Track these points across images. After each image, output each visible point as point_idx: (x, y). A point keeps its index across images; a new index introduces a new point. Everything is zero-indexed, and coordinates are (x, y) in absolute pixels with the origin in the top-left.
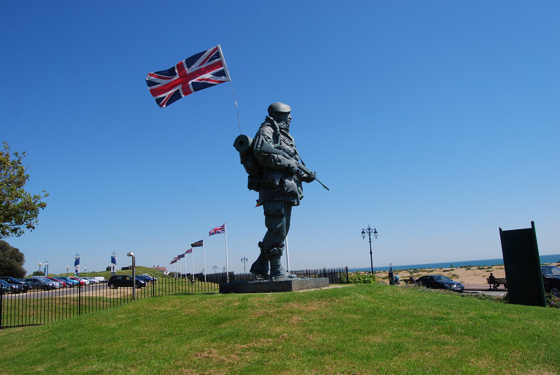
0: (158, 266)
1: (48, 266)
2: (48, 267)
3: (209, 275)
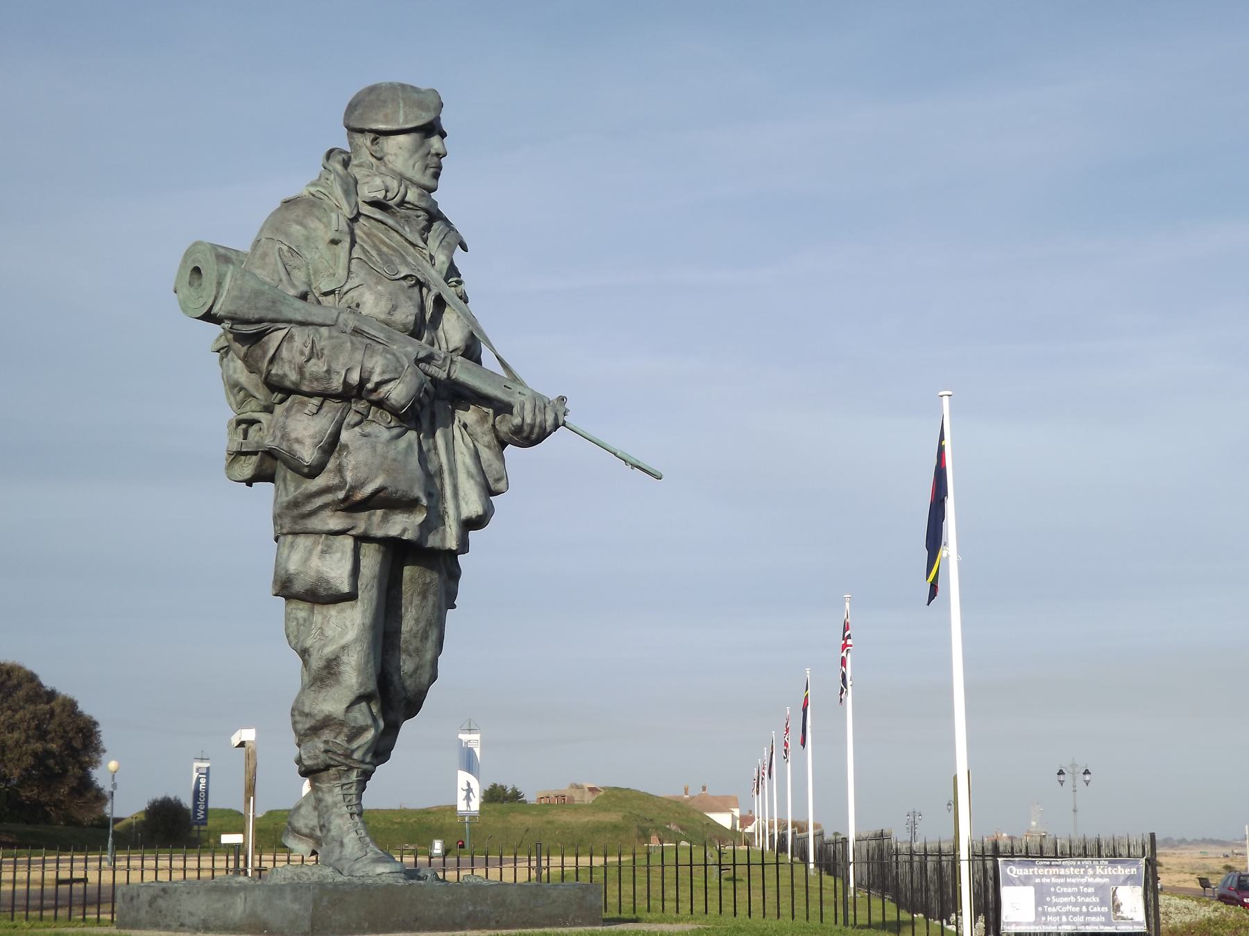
0: (704, 789)
1: (207, 774)
2: (207, 778)
3: (124, 849)
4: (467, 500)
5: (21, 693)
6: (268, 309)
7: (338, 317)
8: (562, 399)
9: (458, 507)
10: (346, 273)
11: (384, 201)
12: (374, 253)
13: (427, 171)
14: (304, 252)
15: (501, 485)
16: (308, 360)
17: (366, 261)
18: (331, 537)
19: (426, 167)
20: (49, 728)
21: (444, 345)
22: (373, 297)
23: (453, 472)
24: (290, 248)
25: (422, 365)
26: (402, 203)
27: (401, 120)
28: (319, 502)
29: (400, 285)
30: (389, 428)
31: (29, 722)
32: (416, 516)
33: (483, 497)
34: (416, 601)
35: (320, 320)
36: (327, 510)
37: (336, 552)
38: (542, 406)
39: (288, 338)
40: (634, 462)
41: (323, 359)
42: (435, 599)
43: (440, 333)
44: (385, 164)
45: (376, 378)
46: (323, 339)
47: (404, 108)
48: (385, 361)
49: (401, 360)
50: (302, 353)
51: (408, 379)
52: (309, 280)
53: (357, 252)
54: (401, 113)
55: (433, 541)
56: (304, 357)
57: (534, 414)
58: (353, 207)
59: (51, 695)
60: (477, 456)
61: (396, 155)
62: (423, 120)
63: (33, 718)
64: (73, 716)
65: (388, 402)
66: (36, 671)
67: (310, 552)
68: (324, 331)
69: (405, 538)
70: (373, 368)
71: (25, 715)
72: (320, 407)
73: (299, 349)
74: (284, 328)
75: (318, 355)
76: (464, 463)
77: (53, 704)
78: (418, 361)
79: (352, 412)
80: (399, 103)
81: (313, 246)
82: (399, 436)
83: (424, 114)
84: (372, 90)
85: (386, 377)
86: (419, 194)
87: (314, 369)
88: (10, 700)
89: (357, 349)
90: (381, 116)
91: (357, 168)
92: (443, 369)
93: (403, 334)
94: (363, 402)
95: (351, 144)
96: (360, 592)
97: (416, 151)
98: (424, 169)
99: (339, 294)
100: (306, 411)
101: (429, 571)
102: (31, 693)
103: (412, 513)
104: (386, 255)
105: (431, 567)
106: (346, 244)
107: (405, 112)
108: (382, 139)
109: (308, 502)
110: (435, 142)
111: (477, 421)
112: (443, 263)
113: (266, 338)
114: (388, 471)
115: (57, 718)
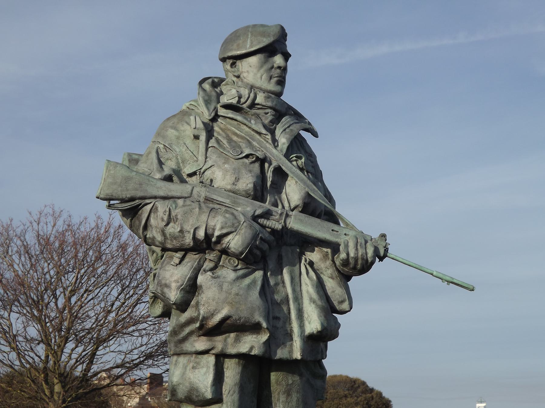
4: (310, 320)
5: (360, 390)
6: (136, 190)
7: (192, 190)
8: (383, 236)
9: (302, 326)
10: (204, 159)
11: (238, 105)
12: (225, 142)
13: (272, 81)
14: (175, 147)
15: (345, 306)
16: (167, 224)
17: (218, 148)
18: (200, 356)
19: (271, 78)
20: (371, 404)
21: (286, 205)
22: (221, 173)
23: (298, 299)
24: (165, 146)
25: (261, 221)
26: (253, 105)
27: (248, 46)
28: (187, 330)
29: (243, 162)
30: (235, 270)
31: (363, 402)
32: (263, 336)
33: (323, 317)
34: (283, 398)
35: (178, 194)
36: (193, 336)
37: (203, 367)
38: (363, 242)
39: (154, 210)
40: (448, 279)
41: (177, 223)
42: (298, 395)
43: (284, 196)
44: (242, 80)
45: (217, 233)
46: (178, 208)
47: (251, 37)
48: (224, 219)
49: (238, 217)
50: (163, 220)
51: (243, 231)
52: (179, 167)
53: (212, 142)
54: (249, 41)
55: (281, 354)
56: (164, 223)
57: (357, 249)
58: (211, 110)
59: (372, 390)
60: (320, 285)
61: (248, 72)
62: (264, 43)
63: (365, 400)
64: (381, 398)
65: (229, 251)
66: (365, 380)
67: (185, 368)
68: (180, 202)
69: (253, 353)
70: (215, 226)
71: (362, 399)
72: (182, 259)
73: (161, 217)
74: (151, 203)
75: (174, 220)
76: (308, 292)
77: (373, 394)
78: (255, 218)
79: (207, 261)
80: (248, 35)
81: (182, 142)
82: (245, 276)
83: (265, 39)
84: (236, 32)
85: (224, 231)
86: (265, 97)
87: (172, 230)
88: (356, 393)
89: (204, 212)
90: (235, 46)
91: (224, 86)
92: (280, 222)
93: (246, 199)
94: (215, 252)
95: (226, 75)
96: (224, 397)
97: (261, 67)
98: (269, 79)
99: (200, 174)
100: (172, 263)
101: (290, 375)
102: (364, 390)
103: (259, 334)
104: (235, 142)
105: (293, 373)
106: (203, 137)
107: (251, 40)
108: (238, 63)
109: (182, 331)
110: (278, 60)
111: (321, 259)
112: (284, 144)
113: (140, 212)
114: (231, 303)
115: (374, 400)
